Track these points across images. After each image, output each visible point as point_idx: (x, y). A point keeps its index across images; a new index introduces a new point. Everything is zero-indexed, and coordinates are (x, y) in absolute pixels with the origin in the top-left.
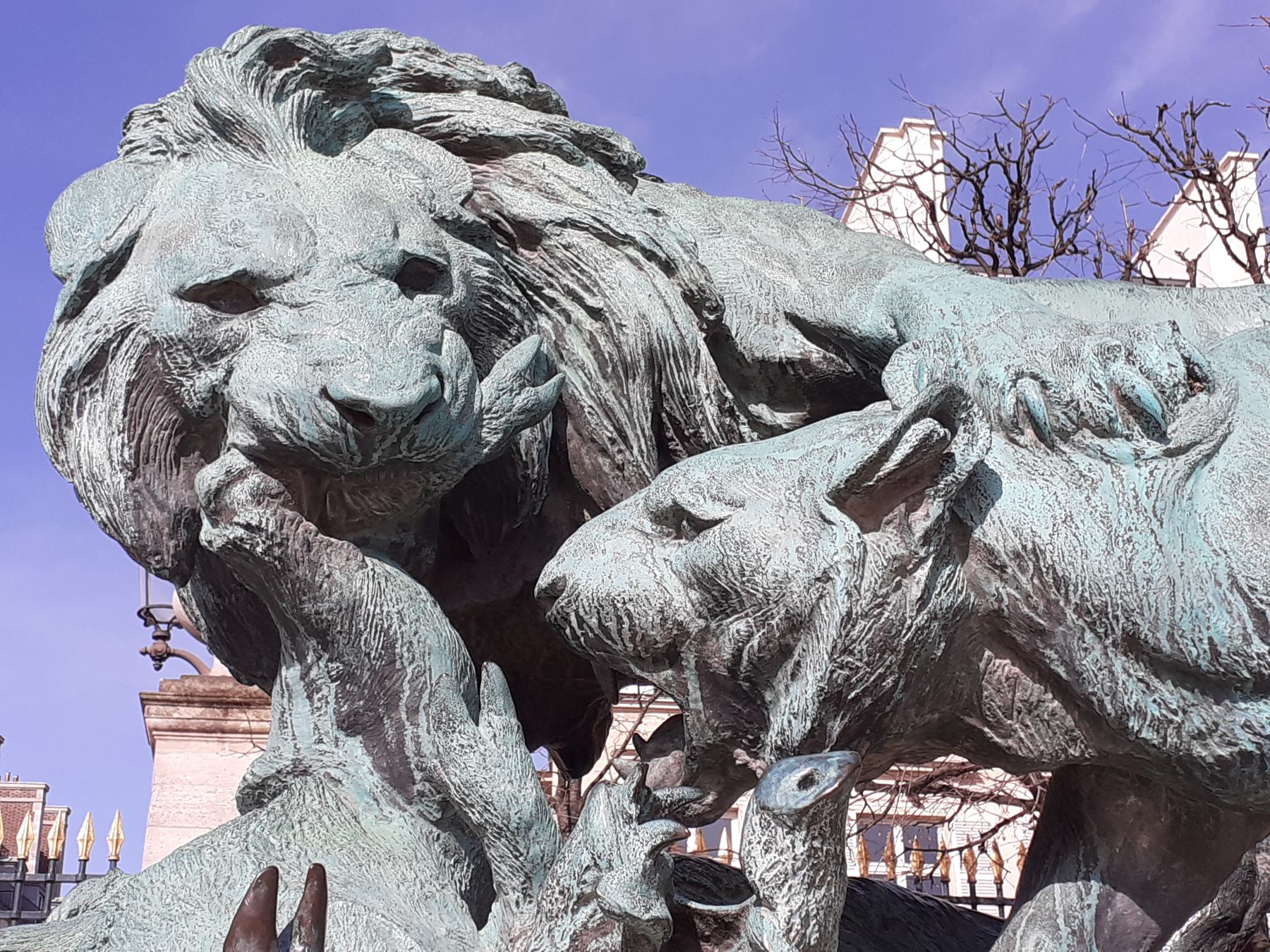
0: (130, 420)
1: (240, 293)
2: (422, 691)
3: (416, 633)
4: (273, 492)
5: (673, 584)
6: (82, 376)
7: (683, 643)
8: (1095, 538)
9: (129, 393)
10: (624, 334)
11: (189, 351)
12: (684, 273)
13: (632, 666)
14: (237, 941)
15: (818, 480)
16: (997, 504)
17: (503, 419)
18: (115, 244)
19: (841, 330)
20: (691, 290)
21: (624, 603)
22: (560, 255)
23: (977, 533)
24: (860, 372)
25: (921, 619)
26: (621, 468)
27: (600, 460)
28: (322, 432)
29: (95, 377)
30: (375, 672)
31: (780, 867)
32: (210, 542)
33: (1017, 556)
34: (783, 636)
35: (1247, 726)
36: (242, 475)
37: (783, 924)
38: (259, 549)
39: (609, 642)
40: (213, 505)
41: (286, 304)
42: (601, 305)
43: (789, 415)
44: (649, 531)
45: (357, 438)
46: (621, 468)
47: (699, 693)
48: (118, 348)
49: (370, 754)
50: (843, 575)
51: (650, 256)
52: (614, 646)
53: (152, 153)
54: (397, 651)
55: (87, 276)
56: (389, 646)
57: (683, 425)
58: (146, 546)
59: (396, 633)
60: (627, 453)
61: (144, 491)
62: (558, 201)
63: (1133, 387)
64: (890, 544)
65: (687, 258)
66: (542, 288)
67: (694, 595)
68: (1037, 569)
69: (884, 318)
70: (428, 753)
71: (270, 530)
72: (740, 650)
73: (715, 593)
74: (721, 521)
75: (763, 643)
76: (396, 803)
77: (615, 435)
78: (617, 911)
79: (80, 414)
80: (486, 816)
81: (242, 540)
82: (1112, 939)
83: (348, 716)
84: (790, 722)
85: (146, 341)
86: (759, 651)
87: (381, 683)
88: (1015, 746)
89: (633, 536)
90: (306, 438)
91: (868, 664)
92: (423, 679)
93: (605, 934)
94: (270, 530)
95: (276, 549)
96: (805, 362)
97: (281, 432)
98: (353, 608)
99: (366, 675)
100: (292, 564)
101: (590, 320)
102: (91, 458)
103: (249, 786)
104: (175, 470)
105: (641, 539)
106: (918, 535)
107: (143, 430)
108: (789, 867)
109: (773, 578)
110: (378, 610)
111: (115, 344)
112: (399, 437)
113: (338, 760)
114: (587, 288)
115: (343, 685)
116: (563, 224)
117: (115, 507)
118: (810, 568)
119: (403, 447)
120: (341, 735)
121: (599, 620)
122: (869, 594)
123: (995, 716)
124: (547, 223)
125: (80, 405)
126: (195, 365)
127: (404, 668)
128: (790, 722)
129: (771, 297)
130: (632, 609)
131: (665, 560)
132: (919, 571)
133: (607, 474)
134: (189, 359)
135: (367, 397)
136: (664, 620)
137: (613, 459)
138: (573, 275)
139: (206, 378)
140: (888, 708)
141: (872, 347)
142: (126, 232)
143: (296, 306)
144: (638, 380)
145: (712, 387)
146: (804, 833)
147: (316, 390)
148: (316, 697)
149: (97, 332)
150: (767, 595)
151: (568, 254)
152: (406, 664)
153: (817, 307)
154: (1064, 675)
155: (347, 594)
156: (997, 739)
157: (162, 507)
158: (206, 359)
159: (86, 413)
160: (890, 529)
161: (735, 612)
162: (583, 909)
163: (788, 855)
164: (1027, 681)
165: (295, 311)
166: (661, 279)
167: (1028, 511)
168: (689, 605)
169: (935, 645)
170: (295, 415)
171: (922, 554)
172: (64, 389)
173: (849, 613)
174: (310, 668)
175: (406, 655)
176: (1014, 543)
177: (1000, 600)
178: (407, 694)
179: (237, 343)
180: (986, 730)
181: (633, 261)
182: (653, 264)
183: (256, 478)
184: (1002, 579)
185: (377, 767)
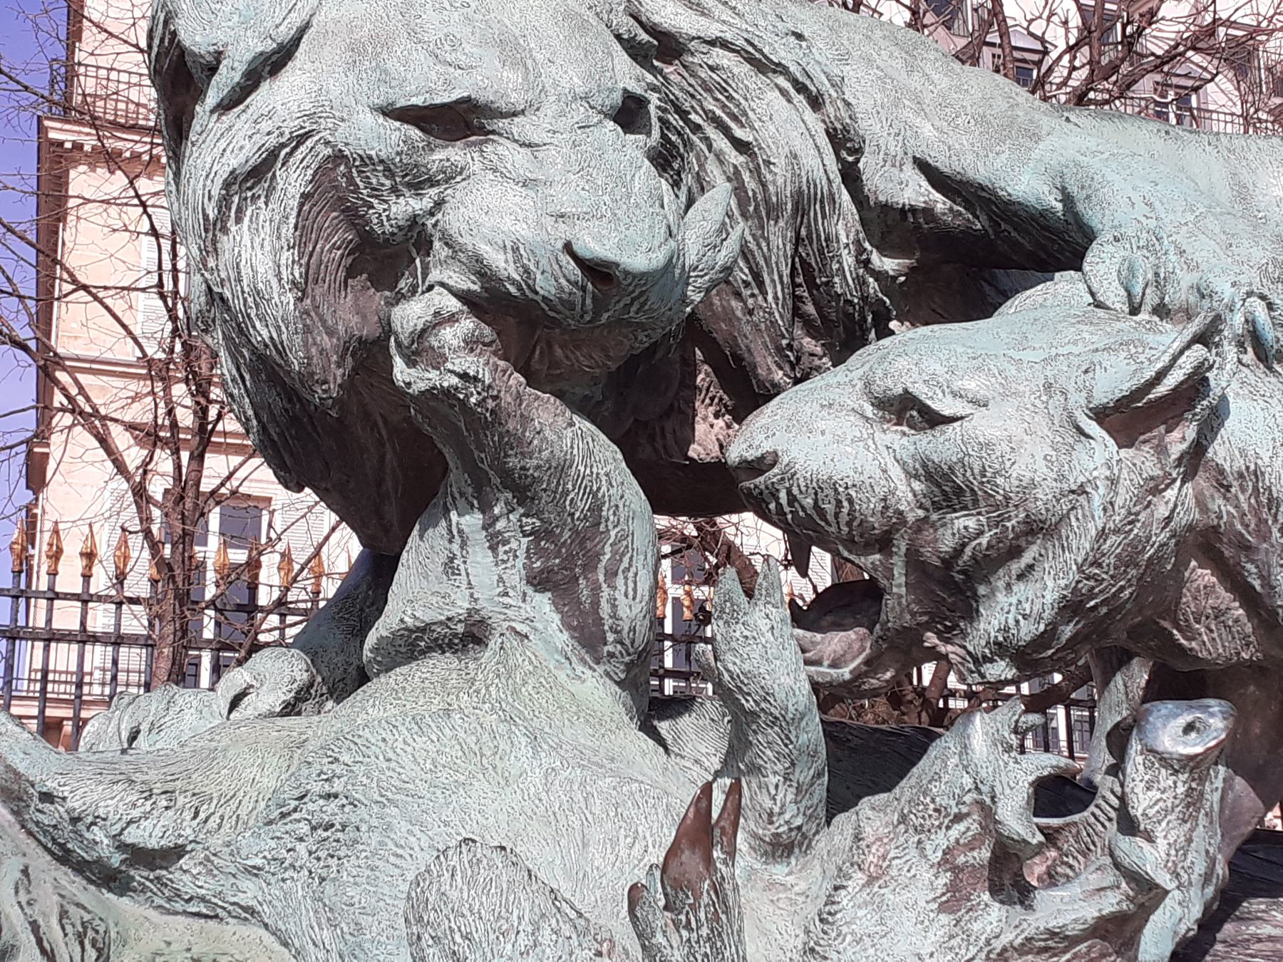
0: (301, 236)
1: (460, 120)
2: (623, 555)
3: (622, 497)
4: (487, 340)
5: (896, 472)
6: (245, 180)
7: (898, 530)
9: (301, 205)
10: (771, 172)
11: (389, 172)
12: (830, 109)
13: (841, 548)
14: (682, 852)
15: (1072, 390)
16: (1226, 424)
17: (707, 278)
18: (285, 33)
19: (981, 187)
20: (835, 129)
21: (847, 488)
22: (703, 75)
23: (1210, 454)
24: (991, 232)
25: (1163, 537)
26: (751, 312)
27: (734, 303)
28: (561, 288)
29: (259, 181)
30: (578, 533)
31: (1161, 804)
32: (409, 384)
33: (1241, 475)
34: (1017, 537)
36: (452, 319)
37: (1164, 856)
38: (473, 400)
39: (823, 524)
40: (415, 345)
41: (516, 141)
42: (751, 139)
43: (896, 261)
44: (871, 416)
45: (594, 298)
46: (751, 312)
47: (904, 579)
49: (558, 610)
50: (1102, 491)
51: (801, 88)
52: (827, 528)
54: (604, 513)
55: (253, 66)
56: (596, 508)
57: (816, 273)
58: (313, 374)
59: (604, 496)
60: (760, 298)
61: (313, 314)
62: (703, 14)
64: (1147, 464)
65: (832, 92)
66: (689, 113)
67: (917, 486)
68: (1256, 489)
69: (1046, 189)
70: (624, 617)
71: (487, 382)
72: (964, 545)
73: (947, 489)
74: (962, 418)
75: (994, 542)
76: (585, 663)
77: (750, 278)
78: (1016, 837)
79: (239, 220)
80: (763, 705)
81: (456, 389)
82: (1230, 818)
83: (542, 572)
84: (1017, 622)
85: (329, 151)
86: (987, 549)
87: (582, 543)
88: (1197, 648)
89: (852, 418)
90: (542, 292)
91: (1112, 577)
92: (625, 543)
93: (973, 849)
94: (487, 382)
95: (490, 401)
96: (928, 212)
97: (514, 282)
98: (562, 469)
99: (567, 534)
100: (503, 416)
101: (734, 153)
102: (255, 272)
103: (406, 629)
104: (343, 293)
105: (861, 422)
106: (1174, 457)
107: (314, 248)
108: (1170, 805)
109: (1017, 483)
110: (588, 471)
112: (633, 300)
113: (524, 615)
114: (734, 118)
115: (537, 541)
116: (712, 43)
117: (283, 329)
118: (1061, 478)
119: (634, 309)
120: (530, 591)
121: (816, 501)
122: (1123, 511)
123: (1187, 621)
124: (694, 38)
125: (240, 211)
126: (394, 190)
127: (608, 531)
128: (1017, 622)
129: (900, 138)
130: (854, 494)
131: (888, 448)
132: (1169, 491)
133: (739, 319)
134: (388, 183)
135: (617, 259)
136: (886, 508)
137: (745, 304)
138: (716, 100)
139: (404, 206)
140: (1119, 617)
141: (1021, 213)
142: (296, 20)
143: (530, 146)
144: (781, 223)
145: (851, 237)
146: (1186, 775)
147: (560, 245)
148: (501, 549)
149: (269, 134)
150: (1007, 498)
151: (714, 76)
152: (610, 527)
153: (954, 158)
154: (1258, 588)
155: (557, 452)
156: (1182, 641)
157: (331, 333)
158: (409, 185)
159: (246, 220)
160: (1146, 448)
161: (965, 508)
162: (956, 826)
163: (1170, 794)
164: (1220, 590)
165: (528, 151)
166: (809, 115)
167: (1252, 433)
168: (910, 495)
169: (1167, 560)
171: (1174, 475)
172: (224, 192)
173: (1104, 529)
174: (497, 519)
175: (611, 518)
176: (1240, 464)
177: (1220, 517)
178: (607, 557)
179: (451, 175)
180: (1175, 632)
181: (783, 92)
182: (801, 97)
183: (468, 324)
184: (1225, 498)
185: (566, 625)
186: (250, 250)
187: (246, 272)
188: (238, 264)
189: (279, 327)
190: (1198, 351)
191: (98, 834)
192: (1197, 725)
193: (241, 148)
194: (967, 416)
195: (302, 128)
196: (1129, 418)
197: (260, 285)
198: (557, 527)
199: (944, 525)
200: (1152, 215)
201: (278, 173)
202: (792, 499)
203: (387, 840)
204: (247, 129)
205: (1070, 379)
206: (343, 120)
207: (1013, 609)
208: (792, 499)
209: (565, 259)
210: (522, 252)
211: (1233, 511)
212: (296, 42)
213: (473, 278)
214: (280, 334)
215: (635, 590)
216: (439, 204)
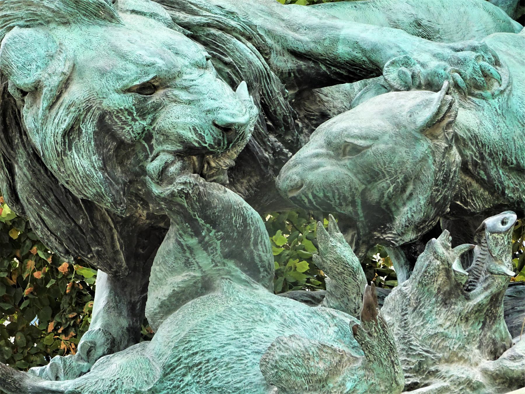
2: (258, 237)
5: (350, 174)
36: (173, 162)
48: (85, 117)
49: (237, 266)
51: (243, 35)
52: (331, 203)
53: (26, 21)
56: (245, 219)
63: (489, 70)
67: (360, 176)
68: (477, 143)
70: (265, 260)
79: (70, 149)
84: (412, 216)
87: (242, 236)
97: (196, 141)
99: (235, 234)
102: (84, 168)
111: (83, 116)
112: (240, 136)
114: (223, 54)
117: (102, 187)
126: (134, 120)
128: (412, 216)
134: (130, 118)
136: (351, 189)
139: (140, 124)
148: (209, 249)
151: (208, 39)
153: (305, 46)
157: (118, 183)
170: (203, 134)
174: (205, 237)
178: (253, 239)
179: (157, 107)
183: (178, 164)
186: (79, 160)
187: (80, 169)
188: (76, 167)
189: (100, 187)
192: (505, 221)
193: (65, 120)
194: (372, 145)
195: (87, 105)
197: (88, 172)
198: (231, 233)
199: (374, 188)
200: (400, 50)
201: (81, 126)
202: (314, 196)
203: (232, 357)
206: (104, 98)
207: (409, 212)
208: (314, 196)
209: (214, 128)
210: (197, 129)
211: (471, 153)
213: (179, 145)
214: (101, 190)
215: (266, 249)
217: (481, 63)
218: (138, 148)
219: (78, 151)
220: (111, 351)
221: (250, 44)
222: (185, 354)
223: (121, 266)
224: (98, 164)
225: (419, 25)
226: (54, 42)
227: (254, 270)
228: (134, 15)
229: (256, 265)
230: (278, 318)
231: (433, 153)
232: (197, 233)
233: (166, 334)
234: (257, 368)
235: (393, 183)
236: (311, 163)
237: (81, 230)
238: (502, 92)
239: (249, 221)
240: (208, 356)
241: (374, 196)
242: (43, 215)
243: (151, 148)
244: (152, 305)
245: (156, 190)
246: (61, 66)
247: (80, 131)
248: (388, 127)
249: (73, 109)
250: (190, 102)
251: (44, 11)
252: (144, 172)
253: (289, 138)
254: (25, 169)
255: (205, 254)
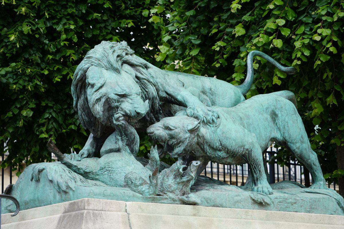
1: (124, 96)
5: (166, 135)
8: (208, 135)
12: (156, 87)
18: (103, 83)
35: (217, 154)
36: (121, 117)
51: (153, 84)
56: (135, 137)
79: (97, 104)
96: (166, 98)
118: (184, 137)
179: (122, 101)
183: (123, 118)
187: (97, 110)
190: (199, 125)
191: (81, 170)
196: (192, 131)
204: (99, 94)
205: (185, 126)
212: (104, 85)
216: (120, 104)
217: (213, 117)
218: (114, 109)
219: (98, 105)
220: (87, 157)
221: (154, 88)
222: (107, 166)
223: (98, 135)
224: (102, 110)
225: (211, 90)
226: (102, 74)
227: (132, 151)
228: (125, 73)
229: (133, 149)
230: (133, 166)
231: (189, 138)
232: (121, 136)
233: (103, 160)
234: (124, 177)
235: (177, 141)
236: (157, 129)
237: (91, 122)
238: (216, 126)
239: (136, 138)
240: (113, 169)
241: (170, 143)
242: (82, 114)
243: (117, 111)
244: (103, 149)
245: (115, 122)
246: (101, 82)
247: (101, 100)
248: (181, 127)
249: (101, 94)
250: (131, 103)
251: (103, 64)
252: (113, 115)
253: (156, 116)
254: (82, 101)
255: (121, 142)
